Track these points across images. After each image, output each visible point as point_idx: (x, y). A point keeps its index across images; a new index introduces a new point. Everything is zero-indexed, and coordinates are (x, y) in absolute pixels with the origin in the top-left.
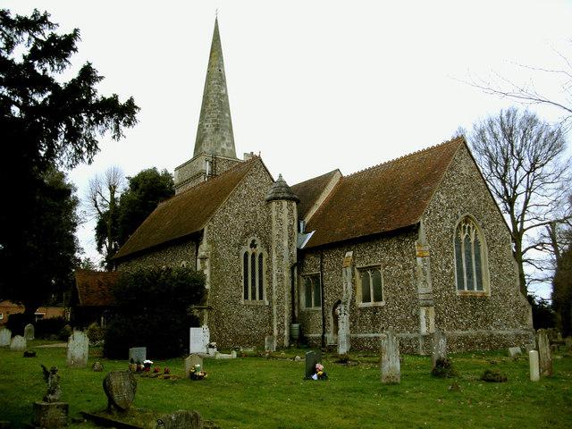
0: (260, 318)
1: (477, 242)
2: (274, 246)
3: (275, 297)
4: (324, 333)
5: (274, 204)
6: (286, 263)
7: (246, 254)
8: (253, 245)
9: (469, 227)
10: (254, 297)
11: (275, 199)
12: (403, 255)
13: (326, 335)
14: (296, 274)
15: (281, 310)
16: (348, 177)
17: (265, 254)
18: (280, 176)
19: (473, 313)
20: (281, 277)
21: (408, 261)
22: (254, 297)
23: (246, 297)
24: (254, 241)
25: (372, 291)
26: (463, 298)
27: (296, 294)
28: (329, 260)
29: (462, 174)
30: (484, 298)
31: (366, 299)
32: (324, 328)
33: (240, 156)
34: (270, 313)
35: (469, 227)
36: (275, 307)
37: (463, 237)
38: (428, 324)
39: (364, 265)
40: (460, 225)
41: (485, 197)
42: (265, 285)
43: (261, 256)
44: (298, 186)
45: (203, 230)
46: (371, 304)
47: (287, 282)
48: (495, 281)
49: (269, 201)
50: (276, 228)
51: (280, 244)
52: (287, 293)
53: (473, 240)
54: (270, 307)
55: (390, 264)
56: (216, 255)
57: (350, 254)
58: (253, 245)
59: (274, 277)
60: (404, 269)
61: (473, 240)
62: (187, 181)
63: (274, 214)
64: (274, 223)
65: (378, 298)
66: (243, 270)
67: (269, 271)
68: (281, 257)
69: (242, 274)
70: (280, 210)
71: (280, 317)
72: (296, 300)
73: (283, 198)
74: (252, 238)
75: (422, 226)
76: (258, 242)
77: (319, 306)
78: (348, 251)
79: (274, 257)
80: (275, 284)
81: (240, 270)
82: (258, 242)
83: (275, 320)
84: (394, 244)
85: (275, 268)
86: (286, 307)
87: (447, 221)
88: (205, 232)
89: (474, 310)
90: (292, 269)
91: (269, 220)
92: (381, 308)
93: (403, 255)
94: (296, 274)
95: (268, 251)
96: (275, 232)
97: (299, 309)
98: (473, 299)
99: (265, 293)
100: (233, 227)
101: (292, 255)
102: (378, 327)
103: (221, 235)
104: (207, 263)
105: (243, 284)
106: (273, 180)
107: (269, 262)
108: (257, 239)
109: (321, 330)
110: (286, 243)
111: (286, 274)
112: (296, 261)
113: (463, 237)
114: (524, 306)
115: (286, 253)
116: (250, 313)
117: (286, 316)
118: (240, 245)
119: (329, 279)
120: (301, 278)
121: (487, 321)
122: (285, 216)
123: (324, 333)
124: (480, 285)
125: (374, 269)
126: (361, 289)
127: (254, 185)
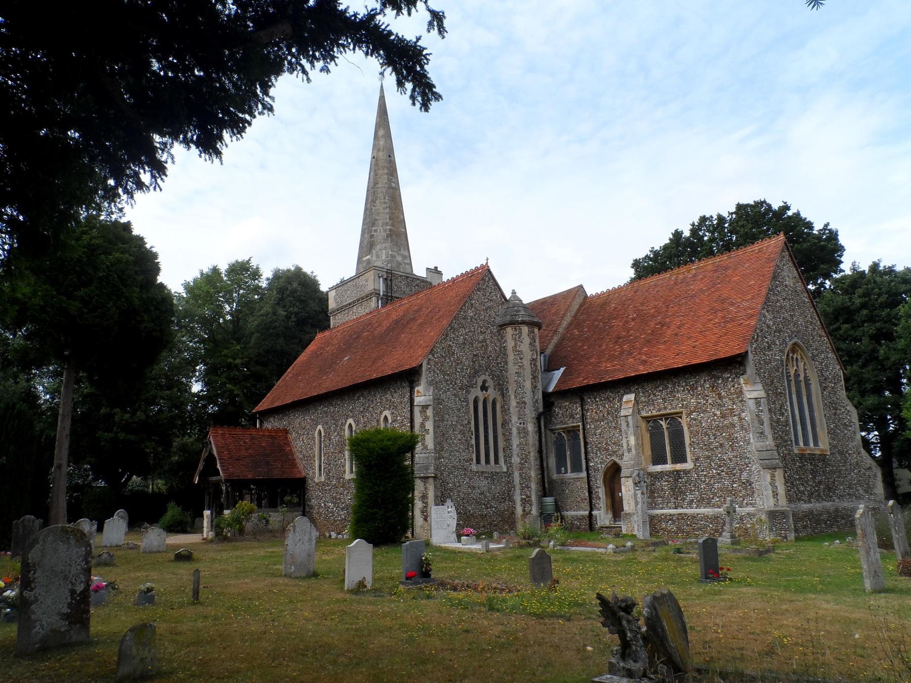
0: (497, 489)
1: (807, 380)
2: (512, 388)
3: (516, 460)
4: (591, 510)
5: (509, 331)
6: (530, 414)
7: (476, 401)
8: (484, 388)
9: (797, 359)
10: (487, 461)
11: (512, 323)
12: (720, 397)
13: (593, 513)
14: (543, 427)
15: (525, 479)
16: (592, 297)
17: (499, 399)
18: (514, 292)
19: (814, 478)
20: (523, 432)
21: (728, 404)
22: (487, 461)
23: (478, 461)
24: (484, 382)
25: (668, 448)
26: (802, 456)
27: (544, 456)
28: (596, 408)
29: (786, 286)
30: (823, 457)
31: (659, 459)
32: (591, 502)
33: (419, 271)
34: (510, 483)
35: (797, 359)
36: (516, 475)
37: (792, 372)
38: (320, 475)
39: (655, 413)
40: (788, 355)
41: (812, 318)
42: (501, 444)
43: (494, 403)
44: (598, 296)
45: (421, 365)
46: (669, 467)
47: (532, 438)
48: (832, 433)
49: (503, 326)
50: (515, 364)
51: (520, 386)
52: (533, 455)
53: (802, 378)
54: (509, 474)
55: (699, 409)
56: (437, 401)
57: (632, 397)
58: (484, 388)
59: (514, 431)
60: (723, 416)
61: (802, 378)
62: (351, 305)
63: (510, 344)
64: (511, 357)
65: (679, 457)
66: (473, 422)
67: (505, 424)
68: (522, 404)
69: (473, 429)
70: (518, 339)
71: (525, 487)
72: (545, 465)
73: (523, 323)
74: (483, 377)
75: (751, 356)
76: (490, 383)
77: (580, 471)
78: (627, 393)
79: (513, 403)
80: (515, 442)
81: (469, 423)
82: (490, 383)
83: (518, 492)
84: (704, 383)
85: (514, 419)
86: (533, 474)
87: (775, 349)
88: (424, 368)
89: (814, 473)
90: (538, 419)
91: (503, 352)
92: (686, 472)
93: (720, 397)
94: (543, 427)
95: (503, 395)
96: (512, 368)
97: (549, 477)
98: (812, 457)
99: (501, 455)
100: (459, 362)
101: (537, 401)
102: (684, 500)
103: (444, 373)
104: (429, 412)
105: (473, 442)
106: (505, 299)
107: (505, 411)
108: (488, 379)
109: (586, 505)
110: (528, 384)
111: (531, 427)
112: (541, 410)
113: (792, 372)
114: (870, 468)
115: (528, 399)
116: (483, 483)
117: (533, 486)
118: (467, 388)
119: (597, 433)
120: (549, 433)
121: (830, 489)
122: (525, 347)
123: (591, 510)
124: (816, 443)
125: (673, 418)
126: (66, 444)
127: (482, 304)
